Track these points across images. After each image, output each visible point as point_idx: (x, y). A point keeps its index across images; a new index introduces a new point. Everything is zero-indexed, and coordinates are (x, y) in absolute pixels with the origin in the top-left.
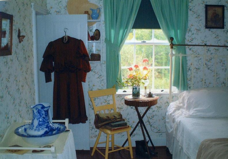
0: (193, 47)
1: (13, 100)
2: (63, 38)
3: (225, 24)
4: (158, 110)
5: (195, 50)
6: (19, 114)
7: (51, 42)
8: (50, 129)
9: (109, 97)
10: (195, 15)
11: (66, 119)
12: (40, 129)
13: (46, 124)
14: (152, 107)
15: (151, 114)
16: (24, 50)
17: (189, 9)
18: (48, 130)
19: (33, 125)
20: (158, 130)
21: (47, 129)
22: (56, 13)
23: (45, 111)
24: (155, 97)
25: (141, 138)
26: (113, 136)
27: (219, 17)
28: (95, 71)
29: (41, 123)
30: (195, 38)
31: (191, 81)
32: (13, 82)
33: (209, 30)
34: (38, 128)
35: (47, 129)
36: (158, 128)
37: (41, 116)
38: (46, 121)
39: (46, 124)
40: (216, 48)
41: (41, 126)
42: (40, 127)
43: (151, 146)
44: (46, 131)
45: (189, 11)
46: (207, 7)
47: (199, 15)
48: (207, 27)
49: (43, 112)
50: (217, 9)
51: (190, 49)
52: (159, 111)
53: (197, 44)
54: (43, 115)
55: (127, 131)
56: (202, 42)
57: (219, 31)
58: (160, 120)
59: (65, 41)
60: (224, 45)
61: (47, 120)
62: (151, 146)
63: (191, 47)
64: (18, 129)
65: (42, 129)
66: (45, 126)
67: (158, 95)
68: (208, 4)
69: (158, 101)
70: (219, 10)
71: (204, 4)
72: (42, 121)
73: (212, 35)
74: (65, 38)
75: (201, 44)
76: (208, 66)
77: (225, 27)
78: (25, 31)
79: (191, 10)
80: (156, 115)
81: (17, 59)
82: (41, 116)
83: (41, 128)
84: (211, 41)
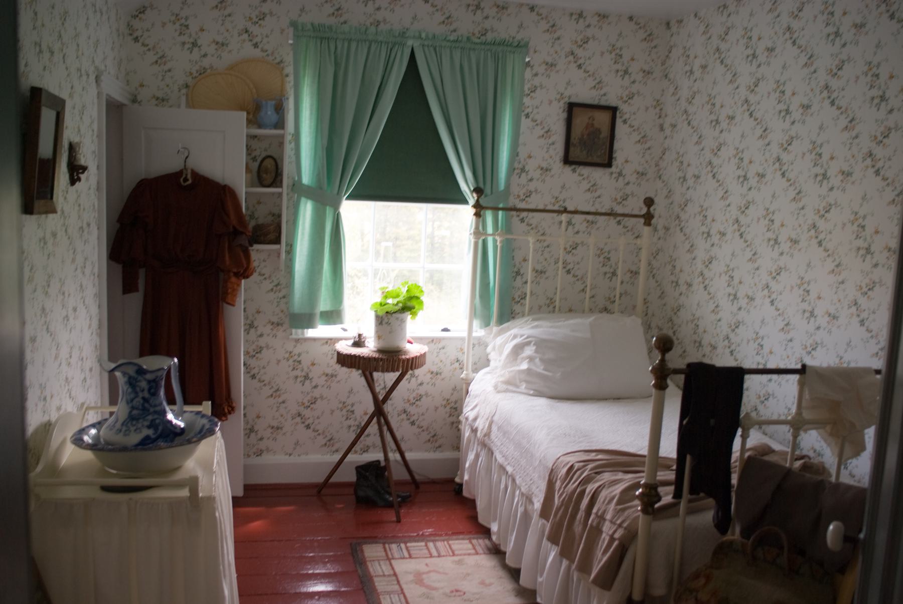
0: (531, 214)
1: (56, 347)
2: (179, 174)
3: (614, 156)
4: (328, 383)
5: (534, 222)
6: (67, 388)
7: (142, 180)
8: (159, 431)
9: (301, 344)
11: (204, 403)
13: (150, 417)
15: (308, 393)
16: (79, 205)
18: (154, 434)
20: (433, 434)
21: (150, 432)
22: (154, 102)
23: (149, 382)
25: (376, 455)
27: (602, 136)
29: (135, 412)
30: (632, 194)
32: (57, 296)
33: (574, 171)
35: (150, 432)
37: (136, 393)
38: (152, 410)
39: (150, 417)
40: (590, 217)
41: (134, 422)
44: (147, 438)
45: (523, 118)
46: (572, 108)
47: (549, 130)
49: (144, 384)
51: (522, 220)
52: (329, 387)
53: (541, 207)
54: (143, 391)
55: (454, 555)
56: (553, 200)
57: (597, 174)
58: (436, 408)
60: (609, 212)
61: (155, 406)
62: (406, 476)
63: (524, 214)
64: (83, 431)
65: (135, 430)
66: (146, 423)
67: (433, 341)
68: (574, 100)
70: (602, 119)
71: (562, 102)
72: (140, 407)
75: (550, 207)
77: (614, 163)
79: (625, 122)
80: (322, 397)
81: (66, 231)
82: (136, 393)
83: (135, 428)
84: (578, 199)
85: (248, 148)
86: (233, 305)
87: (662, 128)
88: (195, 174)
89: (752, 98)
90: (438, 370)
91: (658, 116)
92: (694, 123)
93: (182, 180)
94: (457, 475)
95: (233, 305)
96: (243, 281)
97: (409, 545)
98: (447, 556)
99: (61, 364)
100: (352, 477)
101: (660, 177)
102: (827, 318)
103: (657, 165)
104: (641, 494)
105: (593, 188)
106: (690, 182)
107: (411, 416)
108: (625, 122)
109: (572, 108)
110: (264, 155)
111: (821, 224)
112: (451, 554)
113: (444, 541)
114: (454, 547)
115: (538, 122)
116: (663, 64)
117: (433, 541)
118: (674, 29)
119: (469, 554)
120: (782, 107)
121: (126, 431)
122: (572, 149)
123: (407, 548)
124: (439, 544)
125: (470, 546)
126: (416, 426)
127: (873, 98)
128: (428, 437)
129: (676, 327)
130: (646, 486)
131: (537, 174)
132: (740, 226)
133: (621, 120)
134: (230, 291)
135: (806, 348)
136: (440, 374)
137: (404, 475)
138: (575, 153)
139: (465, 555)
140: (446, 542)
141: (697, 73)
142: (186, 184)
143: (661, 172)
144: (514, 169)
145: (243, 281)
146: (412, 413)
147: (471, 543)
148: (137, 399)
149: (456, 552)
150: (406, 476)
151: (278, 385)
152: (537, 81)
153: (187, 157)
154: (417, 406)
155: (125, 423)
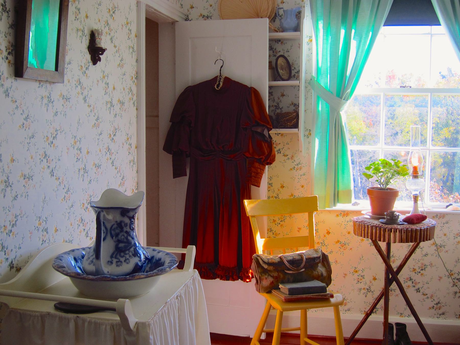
2: (215, 79)
12: (121, 262)
14: (422, 244)
19: (86, 248)
24: (428, 222)
26: (122, 184)
28: (287, 153)
34: (116, 258)
41: (122, 254)
42: (122, 257)
43: (415, 322)
59: (218, 86)
62: (423, 339)
65: (125, 261)
69: (437, 232)
74: (218, 78)
78: (112, 42)
80: (431, 265)
85: (271, 48)
86: (259, 187)
88: (227, 80)
90: (442, 242)
93: (216, 87)
95: (259, 187)
96: (267, 166)
99: (11, 193)
107: (416, 284)
110: (281, 53)
121: (117, 262)
128: (432, 304)
134: (253, 174)
136: (444, 246)
142: (219, 88)
145: (267, 166)
146: (417, 281)
148: (122, 233)
150: (423, 339)
151: (439, 298)
153: (222, 66)
154: (422, 274)
155: (114, 256)
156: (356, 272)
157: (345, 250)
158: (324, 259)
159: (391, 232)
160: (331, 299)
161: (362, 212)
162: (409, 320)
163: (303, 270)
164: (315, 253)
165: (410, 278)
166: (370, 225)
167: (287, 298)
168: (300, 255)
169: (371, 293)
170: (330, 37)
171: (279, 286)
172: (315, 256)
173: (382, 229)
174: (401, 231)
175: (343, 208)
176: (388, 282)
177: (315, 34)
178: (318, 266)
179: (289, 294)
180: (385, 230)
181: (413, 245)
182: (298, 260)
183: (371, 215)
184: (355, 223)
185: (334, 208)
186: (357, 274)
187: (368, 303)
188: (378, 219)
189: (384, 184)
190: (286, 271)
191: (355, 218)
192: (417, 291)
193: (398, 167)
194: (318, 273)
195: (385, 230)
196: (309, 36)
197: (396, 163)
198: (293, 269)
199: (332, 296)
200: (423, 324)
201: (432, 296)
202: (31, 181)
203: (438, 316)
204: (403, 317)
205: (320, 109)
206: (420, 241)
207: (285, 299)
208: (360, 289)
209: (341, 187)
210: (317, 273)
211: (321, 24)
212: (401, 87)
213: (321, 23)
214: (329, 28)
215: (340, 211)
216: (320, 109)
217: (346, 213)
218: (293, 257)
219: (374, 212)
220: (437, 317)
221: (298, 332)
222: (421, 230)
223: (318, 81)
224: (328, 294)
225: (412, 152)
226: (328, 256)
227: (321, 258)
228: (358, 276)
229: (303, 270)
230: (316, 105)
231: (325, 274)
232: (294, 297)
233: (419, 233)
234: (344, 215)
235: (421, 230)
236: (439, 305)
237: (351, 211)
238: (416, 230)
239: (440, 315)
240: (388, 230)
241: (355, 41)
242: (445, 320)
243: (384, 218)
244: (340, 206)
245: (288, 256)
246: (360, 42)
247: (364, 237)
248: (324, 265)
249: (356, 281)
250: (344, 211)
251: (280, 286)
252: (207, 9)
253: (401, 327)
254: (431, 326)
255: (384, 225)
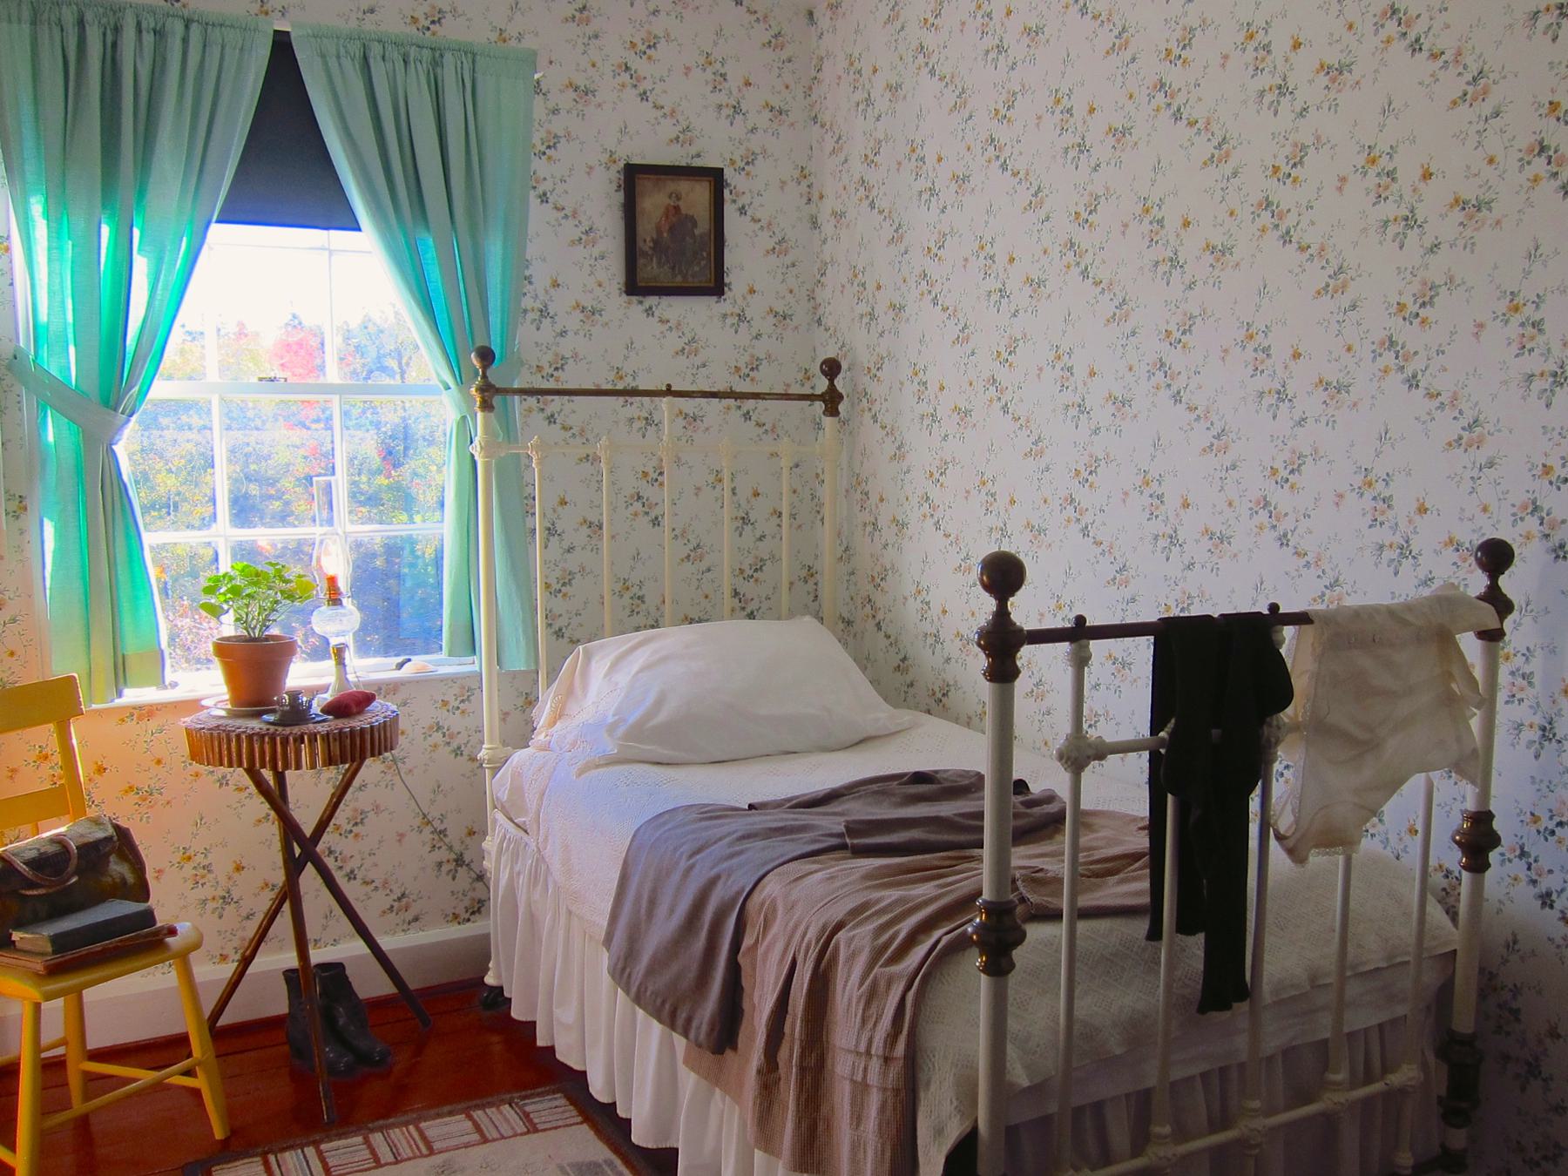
3: (726, 280)
10: (571, 230)
17: (532, 193)
31: (662, 484)
36: (1464, 406)
46: (634, 176)
48: (635, 287)
50: (683, 186)
55: (431, 1152)
62: (386, 987)
68: (636, 161)
70: (697, 197)
73: (664, 337)
76: (344, 860)
77: (728, 294)
80: (377, 809)
87: (815, 223)
89: (1003, 134)
91: (805, 200)
92: (882, 203)
94: (487, 969)
97: (323, 1147)
98: (415, 1157)
100: (278, 1004)
101: (819, 322)
102: (1206, 543)
103: (811, 298)
104: (980, 929)
105: (690, 348)
106: (885, 320)
108: (742, 211)
109: (634, 176)
111: (1175, 358)
112: (424, 1151)
113: (406, 1124)
114: (430, 1133)
115: (667, 110)
116: (807, 95)
117: (380, 1129)
118: (824, 21)
119: (467, 1146)
120: (1070, 139)
122: (641, 261)
123: (320, 1154)
124: (396, 1134)
125: (469, 1124)
126: (359, 881)
127: (1262, 94)
129: (881, 612)
130: (993, 910)
131: (573, 321)
132: (1001, 390)
133: (735, 207)
135: (934, 694)
137: (382, 986)
138: (651, 270)
139: (457, 1148)
140: (411, 1128)
141: (882, 102)
143: (820, 311)
144: (525, 311)
146: (347, 853)
147: (470, 1118)
149: (436, 1146)
152: (558, 125)
154: (356, 835)
156: (189, 858)
157: (152, 807)
158: (122, 842)
159: (303, 742)
160: (169, 940)
161: (204, 703)
162: (347, 949)
163: (74, 879)
164: (95, 828)
165: (438, 723)
166: (243, 732)
167: (52, 962)
168: (58, 841)
169: (233, 905)
170: (70, 242)
171: (11, 934)
172: (100, 835)
173: (278, 738)
174: (326, 737)
175: (138, 699)
176: (293, 868)
177: (20, 230)
178: (109, 862)
179: (54, 952)
180: (285, 742)
181: (347, 770)
182: (56, 855)
183: (229, 707)
184: (189, 732)
185: (118, 702)
186: (192, 864)
187: (228, 934)
188: (258, 715)
189: (255, 627)
190: (23, 892)
191: (188, 720)
192: (350, 878)
193: (287, 582)
194: (113, 879)
195: (285, 742)
196: (1508, 293)
197: (279, 571)
198: (47, 883)
199: (172, 932)
200: (385, 954)
201: (386, 882)
202: (1127, 670)
203: (405, 927)
204: (320, 948)
205: (51, 439)
206: (363, 759)
207: (46, 968)
208: (204, 902)
209: (131, 646)
210: (110, 879)
211: (37, 206)
212: (261, 379)
213: (37, 202)
214: (65, 218)
215: (128, 707)
216: (51, 439)
217: (146, 712)
218: (39, 850)
219: (236, 700)
220: (403, 930)
221: (60, 1051)
222: (372, 727)
223: (38, 361)
224: (162, 927)
225: (321, 542)
226: (128, 829)
227: (115, 838)
228: (195, 868)
229: (74, 879)
230: (38, 430)
231: (130, 878)
232: (69, 955)
233: (368, 737)
234: (140, 718)
235: (372, 727)
236: (404, 900)
237: (159, 704)
238: (362, 730)
239: (409, 923)
240: (295, 740)
241: (145, 260)
242: (421, 933)
243: (273, 711)
244: (133, 695)
245: (23, 849)
246: (160, 260)
247: (230, 765)
248: (123, 857)
249: (190, 884)
250: (140, 708)
251: (16, 936)
252: (779, 93)
253: (335, 970)
254: (401, 951)
255: (280, 729)
